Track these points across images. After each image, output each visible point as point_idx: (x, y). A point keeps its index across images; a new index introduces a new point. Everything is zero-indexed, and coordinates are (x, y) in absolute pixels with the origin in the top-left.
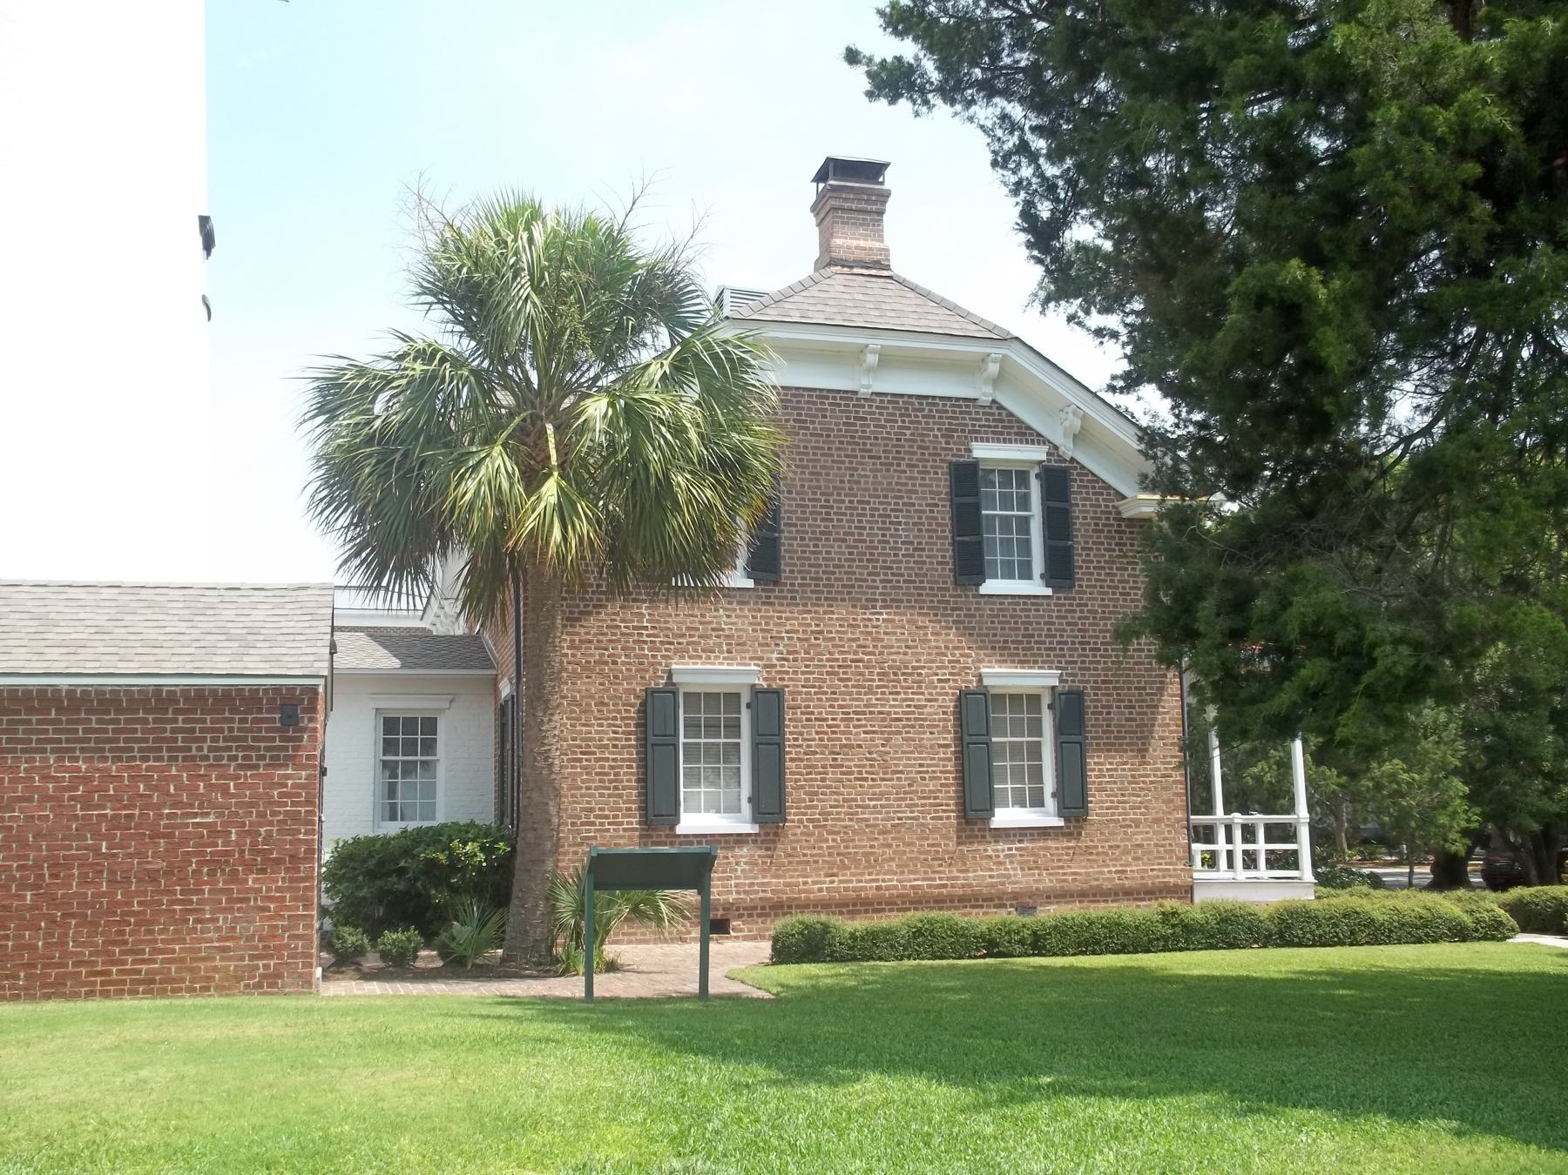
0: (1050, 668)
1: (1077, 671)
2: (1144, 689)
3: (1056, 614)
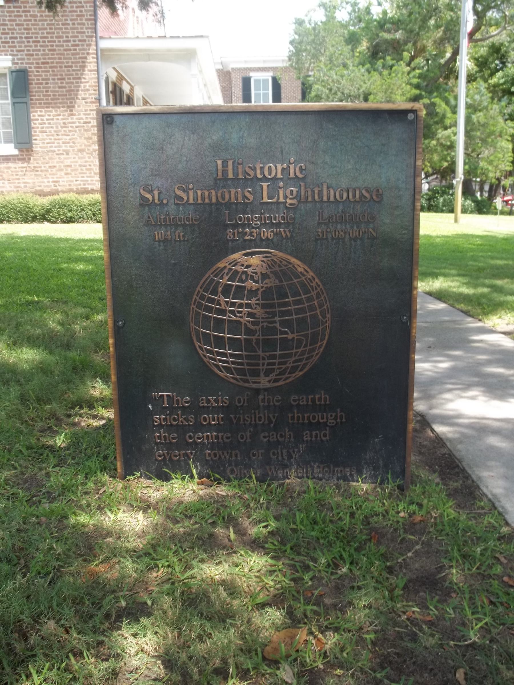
0: (6, 55)
1: (24, 57)
2: (71, 67)
3: (8, 18)
